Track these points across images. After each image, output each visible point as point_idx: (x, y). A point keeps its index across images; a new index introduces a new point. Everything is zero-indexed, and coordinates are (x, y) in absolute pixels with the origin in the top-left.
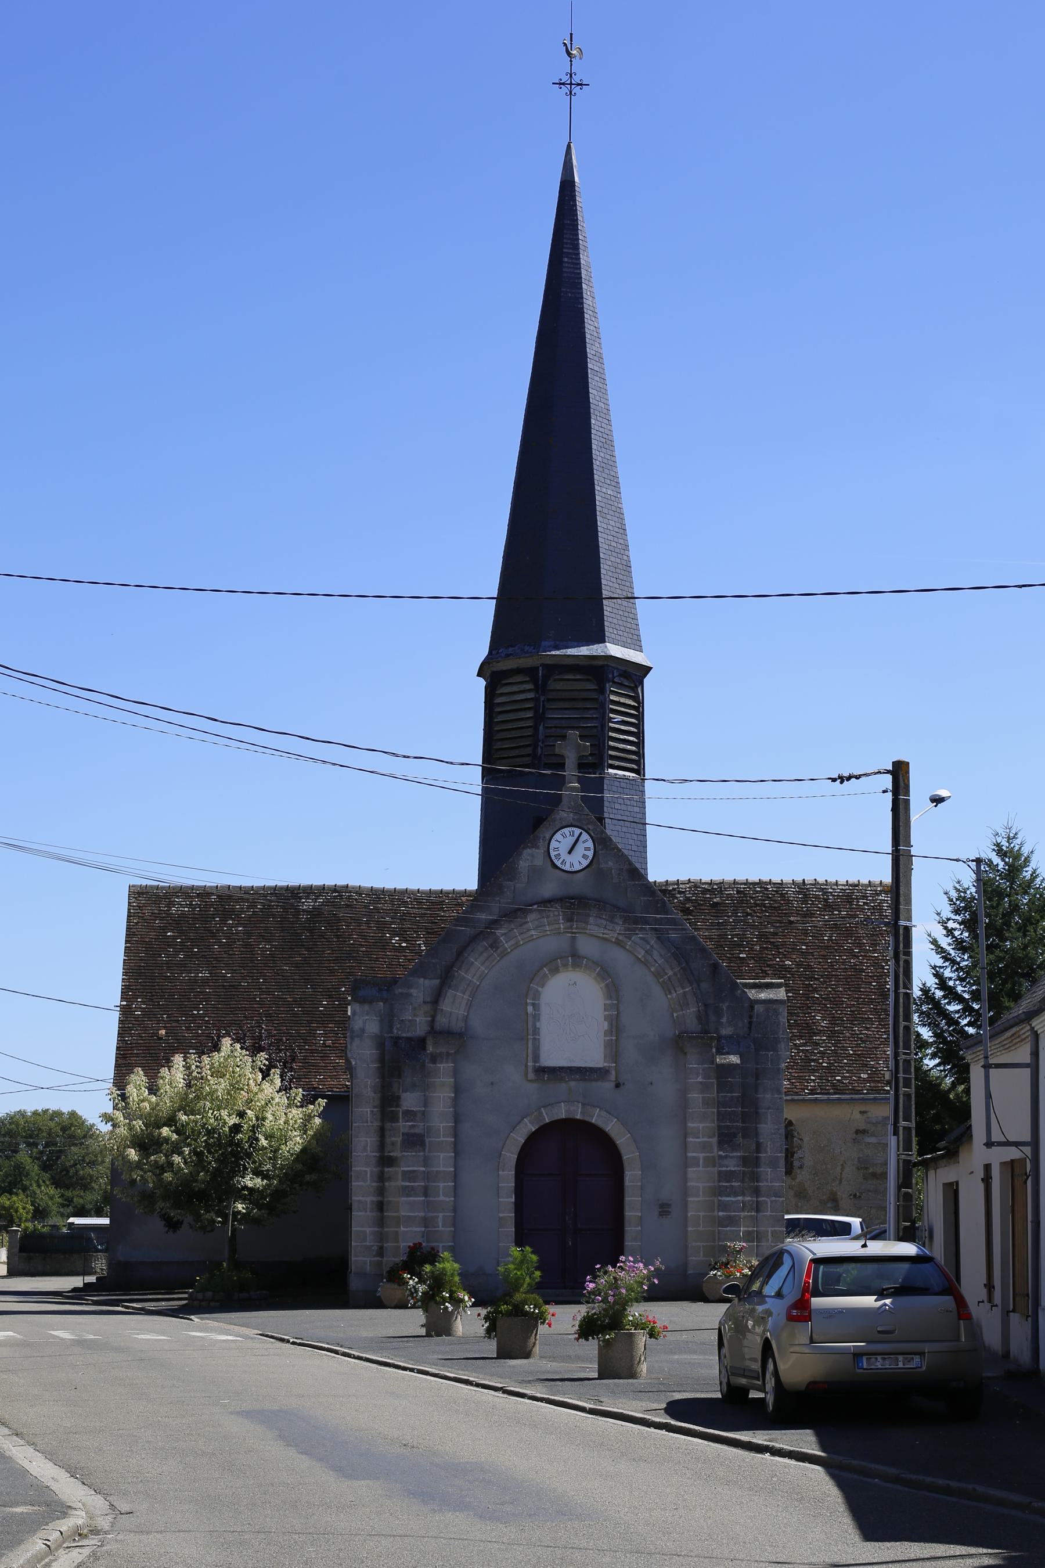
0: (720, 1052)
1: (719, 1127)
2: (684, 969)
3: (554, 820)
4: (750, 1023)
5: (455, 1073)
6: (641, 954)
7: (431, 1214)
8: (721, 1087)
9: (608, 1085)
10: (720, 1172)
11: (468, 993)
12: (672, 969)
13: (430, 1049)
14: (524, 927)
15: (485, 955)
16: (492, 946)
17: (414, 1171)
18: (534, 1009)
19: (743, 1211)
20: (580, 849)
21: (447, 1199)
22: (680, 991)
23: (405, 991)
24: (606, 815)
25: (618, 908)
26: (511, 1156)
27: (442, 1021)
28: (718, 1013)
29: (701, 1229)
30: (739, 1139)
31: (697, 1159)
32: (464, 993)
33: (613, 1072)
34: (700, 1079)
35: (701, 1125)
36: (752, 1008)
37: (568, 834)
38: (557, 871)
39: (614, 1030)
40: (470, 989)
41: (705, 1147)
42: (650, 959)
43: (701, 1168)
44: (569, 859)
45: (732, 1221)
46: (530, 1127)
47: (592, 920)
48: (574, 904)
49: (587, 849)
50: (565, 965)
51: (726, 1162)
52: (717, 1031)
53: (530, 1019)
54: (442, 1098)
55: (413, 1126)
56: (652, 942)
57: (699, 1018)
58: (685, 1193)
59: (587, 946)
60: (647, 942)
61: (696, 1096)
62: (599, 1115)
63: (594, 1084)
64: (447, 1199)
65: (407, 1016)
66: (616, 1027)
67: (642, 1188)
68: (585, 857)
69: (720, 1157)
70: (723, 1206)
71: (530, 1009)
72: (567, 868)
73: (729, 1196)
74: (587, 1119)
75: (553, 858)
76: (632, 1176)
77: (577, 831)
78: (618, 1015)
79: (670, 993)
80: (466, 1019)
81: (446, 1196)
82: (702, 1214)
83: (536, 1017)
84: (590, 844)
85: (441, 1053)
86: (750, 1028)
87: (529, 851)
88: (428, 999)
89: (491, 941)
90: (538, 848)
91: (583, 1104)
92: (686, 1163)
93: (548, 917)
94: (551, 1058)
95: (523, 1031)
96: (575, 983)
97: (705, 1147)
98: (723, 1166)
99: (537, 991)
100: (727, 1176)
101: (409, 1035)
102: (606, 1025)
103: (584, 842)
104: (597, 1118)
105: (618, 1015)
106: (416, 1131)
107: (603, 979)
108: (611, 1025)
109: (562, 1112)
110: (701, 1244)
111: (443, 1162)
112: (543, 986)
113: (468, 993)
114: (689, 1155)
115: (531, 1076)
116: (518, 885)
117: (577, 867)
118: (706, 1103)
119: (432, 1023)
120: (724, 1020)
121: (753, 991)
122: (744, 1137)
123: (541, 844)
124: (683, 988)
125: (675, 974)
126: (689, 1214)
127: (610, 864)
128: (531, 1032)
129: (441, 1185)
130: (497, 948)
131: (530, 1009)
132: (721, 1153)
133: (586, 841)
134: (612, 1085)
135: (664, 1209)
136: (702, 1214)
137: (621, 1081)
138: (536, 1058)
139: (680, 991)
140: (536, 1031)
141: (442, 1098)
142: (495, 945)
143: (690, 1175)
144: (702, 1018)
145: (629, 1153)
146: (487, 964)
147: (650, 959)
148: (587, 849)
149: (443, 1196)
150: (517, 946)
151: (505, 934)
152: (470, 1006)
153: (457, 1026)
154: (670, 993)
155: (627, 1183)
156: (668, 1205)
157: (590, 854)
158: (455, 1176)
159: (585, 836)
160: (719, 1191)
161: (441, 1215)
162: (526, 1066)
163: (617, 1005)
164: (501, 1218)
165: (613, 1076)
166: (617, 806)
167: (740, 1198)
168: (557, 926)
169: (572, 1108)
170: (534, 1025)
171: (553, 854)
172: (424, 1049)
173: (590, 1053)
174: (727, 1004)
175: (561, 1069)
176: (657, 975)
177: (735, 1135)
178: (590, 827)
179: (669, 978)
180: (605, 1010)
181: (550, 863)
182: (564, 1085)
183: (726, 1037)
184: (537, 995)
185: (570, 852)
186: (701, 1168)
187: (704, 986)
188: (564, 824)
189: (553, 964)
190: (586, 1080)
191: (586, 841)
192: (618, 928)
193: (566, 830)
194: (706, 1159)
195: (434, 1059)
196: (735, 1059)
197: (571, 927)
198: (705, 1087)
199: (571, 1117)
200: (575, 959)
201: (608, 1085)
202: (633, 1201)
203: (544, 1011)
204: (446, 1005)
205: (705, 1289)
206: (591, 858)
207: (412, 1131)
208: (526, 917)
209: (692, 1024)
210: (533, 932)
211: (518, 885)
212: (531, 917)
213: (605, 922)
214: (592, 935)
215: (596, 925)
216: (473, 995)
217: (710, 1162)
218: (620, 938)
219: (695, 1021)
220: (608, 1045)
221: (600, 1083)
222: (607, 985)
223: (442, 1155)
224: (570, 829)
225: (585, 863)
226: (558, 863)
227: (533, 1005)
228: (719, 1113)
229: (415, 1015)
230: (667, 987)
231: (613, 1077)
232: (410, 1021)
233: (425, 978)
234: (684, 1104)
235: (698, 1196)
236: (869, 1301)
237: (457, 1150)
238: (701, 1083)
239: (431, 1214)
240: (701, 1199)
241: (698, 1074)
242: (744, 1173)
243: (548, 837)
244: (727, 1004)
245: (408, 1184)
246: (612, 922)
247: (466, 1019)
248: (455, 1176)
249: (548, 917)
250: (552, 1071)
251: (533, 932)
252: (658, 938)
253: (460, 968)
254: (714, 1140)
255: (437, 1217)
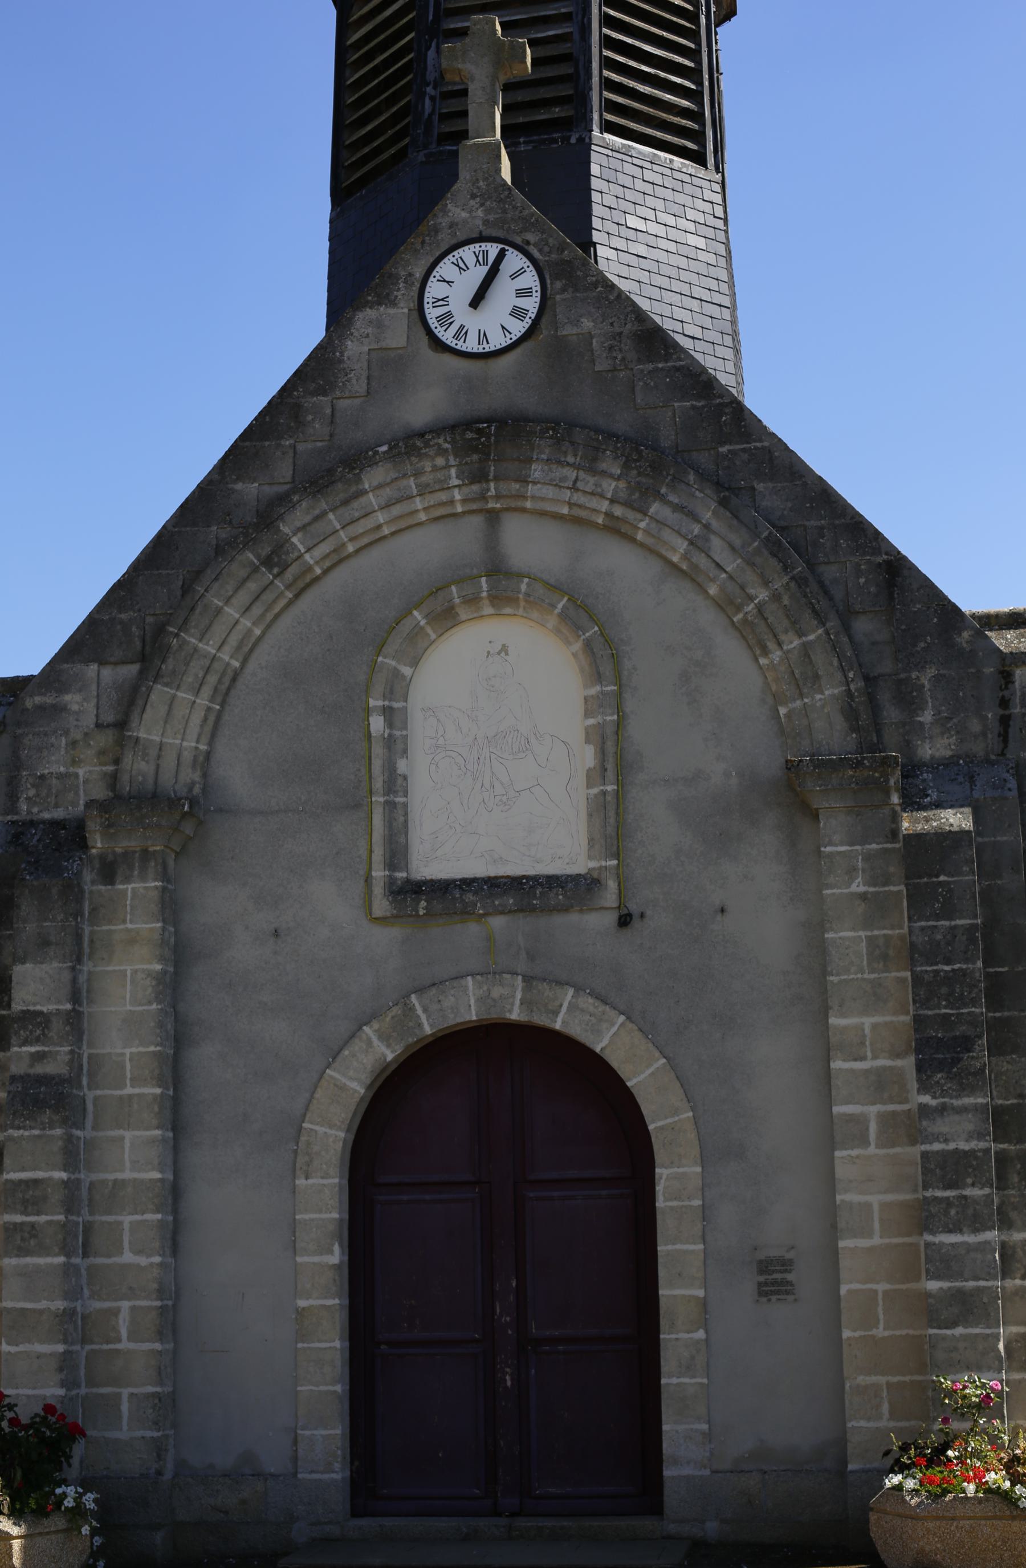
0: (913, 802)
1: (918, 1020)
2: (800, 581)
3: (436, 230)
4: (1005, 721)
5: (171, 907)
6: (677, 549)
7: (98, 1305)
8: (921, 900)
9: (599, 921)
10: (925, 1155)
11: (207, 691)
12: (766, 583)
13: (98, 843)
14: (355, 504)
15: (252, 586)
16: (268, 562)
17: (36, 1182)
18: (390, 724)
19: (1006, 1273)
20: (504, 295)
21: (143, 1261)
22: (793, 643)
23: (48, 699)
24: (596, 237)
25: (611, 435)
26: (330, 1135)
27: (138, 768)
28: (908, 699)
29: (880, 1332)
30: (981, 1055)
31: (860, 1121)
32: (197, 693)
33: (612, 885)
34: (858, 886)
35: (868, 1021)
36: (1006, 677)
37: (470, 260)
38: (447, 358)
39: (610, 766)
40: (212, 679)
41: (881, 1084)
42: (702, 561)
43: (872, 1150)
44: (473, 322)
45: (968, 1307)
46: (378, 1050)
47: (537, 471)
48: (489, 439)
49: (523, 293)
50: (472, 601)
51: (941, 1126)
52: (907, 747)
53: (378, 750)
54: (127, 979)
55: (39, 1057)
56: (707, 516)
57: (850, 714)
58: (831, 1223)
59: (529, 544)
60: (695, 517)
61: (848, 937)
62: (572, 1007)
63: (559, 920)
64: (143, 1261)
65: (54, 765)
66: (615, 759)
67: (706, 1213)
68: (517, 313)
69: (923, 1108)
70: (943, 1264)
71: (377, 724)
72: (471, 345)
73: (956, 1229)
74: (541, 1019)
75: (433, 323)
76: (676, 1180)
77: (493, 250)
78: (620, 725)
79: (765, 652)
80: (205, 761)
81: (138, 1252)
82: (881, 1287)
83: (396, 746)
84: (530, 279)
85: (127, 855)
86: (1004, 737)
87: (370, 313)
88: (109, 717)
89: (266, 550)
90: (393, 303)
91: (528, 979)
92: (830, 1135)
93: (417, 474)
94: (435, 859)
95: (368, 785)
96: (504, 649)
97: (881, 1084)
98: (936, 1138)
99: (396, 673)
100: (949, 1169)
101: (59, 814)
102: (588, 756)
103: (513, 277)
104: (568, 1015)
105: (620, 725)
106: (48, 1068)
107: (578, 628)
108: (602, 753)
109: (467, 1005)
110: (882, 1380)
111: (131, 1155)
112: (415, 663)
113: (207, 691)
114: (218, 707)
115: (381, 906)
116: (342, 404)
117: (497, 341)
118: (880, 954)
119: (113, 779)
120: (927, 717)
121: (1010, 635)
122: (996, 1049)
123: (404, 295)
124: (800, 634)
125: (776, 597)
126: (844, 1289)
127: (587, 324)
128: (378, 784)
129: (127, 1220)
130: (284, 567)
131: (377, 724)
132: (926, 1099)
133: (521, 272)
134: (610, 919)
135: (773, 1279)
136: (881, 1287)
137: (633, 907)
138: (397, 853)
139: (793, 643)
140: (395, 784)
141: (127, 979)
142: (276, 560)
143: (840, 1172)
144: (863, 713)
145: (664, 1112)
146: (257, 610)
147: (702, 561)
148: (523, 293)
149: (132, 1246)
150: (338, 559)
151: (303, 528)
152: (214, 725)
153: (178, 776)
154: (765, 652)
155: (661, 1203)
156: (786, 1265)
157: (531, 304)
158: (174, 1194)
159: (514, 260)
160: (925, 1217)
161: (125, 1305)
162: (368, 879)
163: (619, 695)
164: (301, 1313)
165: (610, 896)
166: (632, 222)
167: (992, 1235)
168: (443, 496)
169: (497, 992)
170: (390, 769)
171: (432, 314)
172: (82, 843)
173: (553, 837)
174: (931, 671)
175: (467, 883)
176: (726, 605)
177: (966, 1043)
178: (531, 237)
179: (760, 608)
180: (588, 714)
181: (425, 339)
182: (473, 928)
183: (936, 766)
184: (397, 688)
185: (477, 301)
186: (872, 1150)
187: (863, 626)
188: (461, 236)
189: (442, 602)
190: (533, 909)
191: (521, 272)
192: (609, 487)
193: (467, 253)
194: (887, 1121)
195: (109, 871)
196: (956, 819)
197: (483, 497)
198: (876, 908)
199: (494, 1015)
200: (498, 582)
201: (599, 921)
202: (677, 1247)
203: (421, 731)
204: (148, 729)
205: (875, 1532)
206: (533, 313)
207: (39, 1069)
208: (358, 480)
209: (824, 711)
210: (381, 517)
211: (342, 404)
212: (373, 477)
213: (572, 474)
214: (543, 514)
215: (548, 482)
216: (224, 695)
217: (910, 1127)
218: (618, 511)
219: (840, 723)
220: (598, 807)
221: (574, 917)
222: (588, 645)
223: (128, 1135)
224: (476, 247)
225: (518, 328)
226: (447, 336)
227: (388, 712)
228: (917, 980)
229: (75, 762)
230: (755, 637)
231: (610, 896)
232: (60, 776)
233: (102, 663)
234: (816, 956)
235: (870, 1235)
236: (431, 18)
237: (177, 1119)
238: (863, 897)
239: (98, 1305)
240: (876, 1241)
241: (851, 872)
242: (1002, 1159)
243: (418, 274)
244: (931, 671)
245: (19, 1218)
246: (593, 471)
247: (205, 761)
248: (174, 1194)
249: (417, 474)
250: (441, 890)
251: (381, 517)
252: (723, 503)
253: (184, 626)
254: (908, 1063)
255: (116, 1312)
